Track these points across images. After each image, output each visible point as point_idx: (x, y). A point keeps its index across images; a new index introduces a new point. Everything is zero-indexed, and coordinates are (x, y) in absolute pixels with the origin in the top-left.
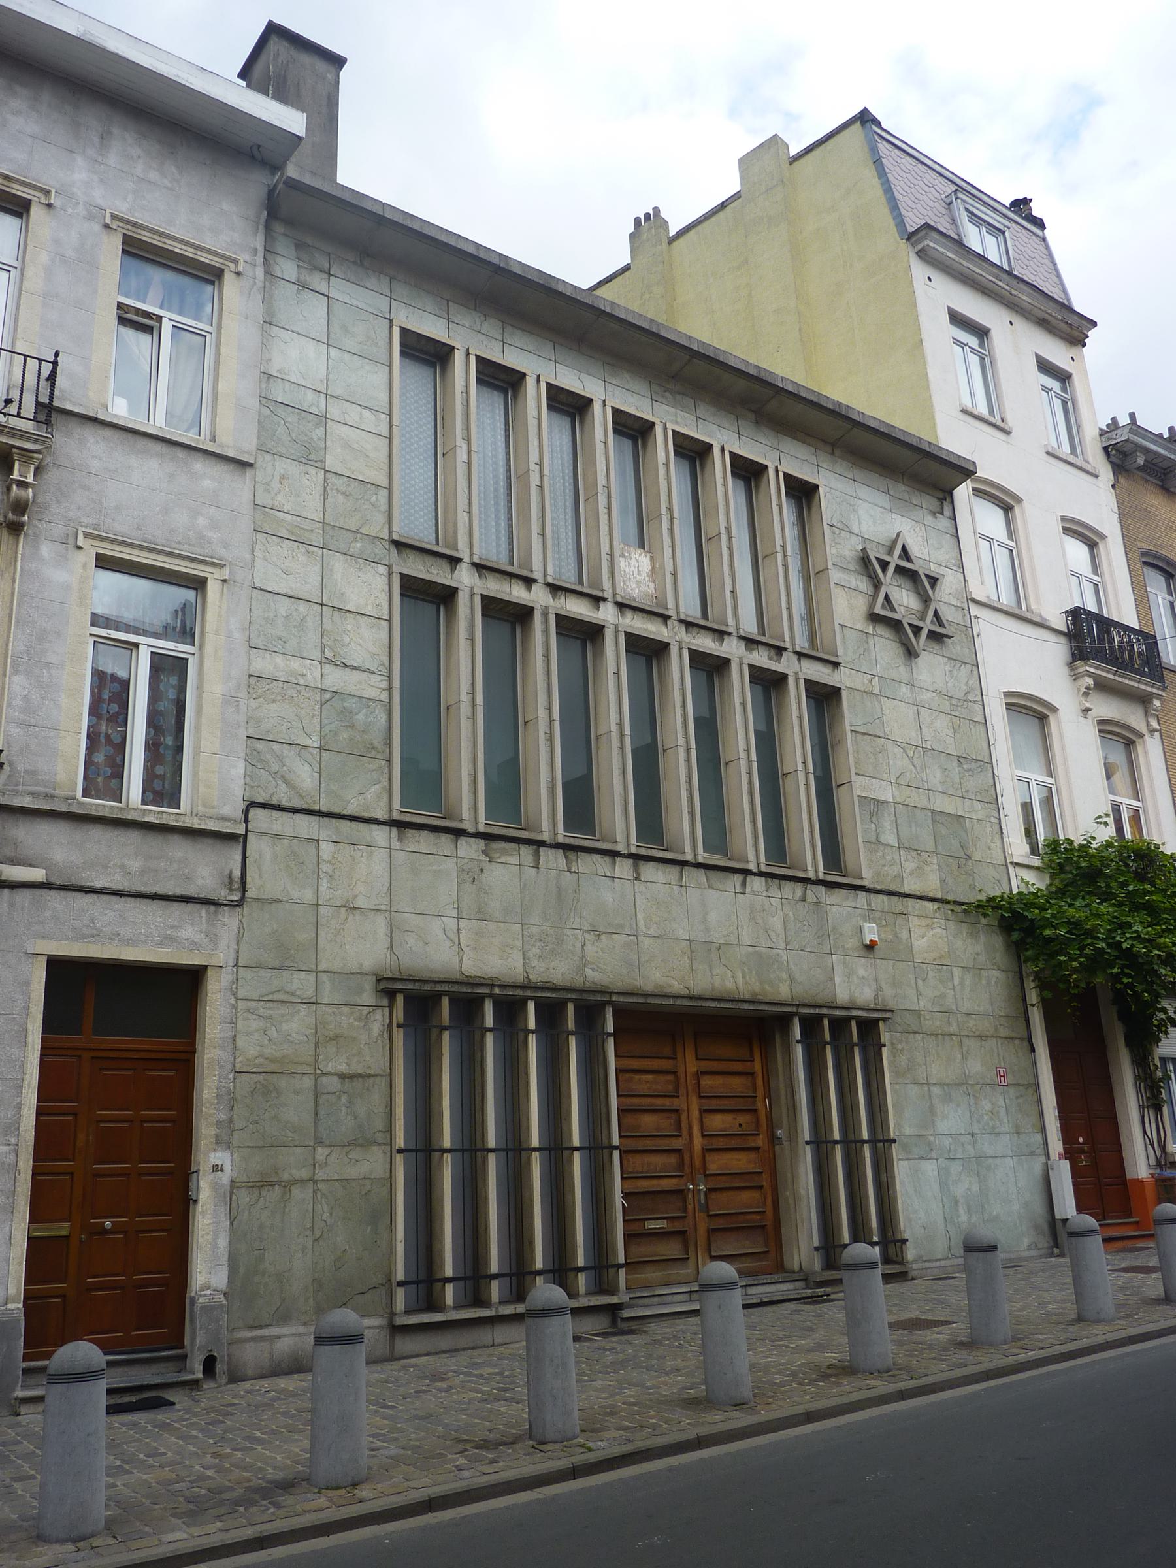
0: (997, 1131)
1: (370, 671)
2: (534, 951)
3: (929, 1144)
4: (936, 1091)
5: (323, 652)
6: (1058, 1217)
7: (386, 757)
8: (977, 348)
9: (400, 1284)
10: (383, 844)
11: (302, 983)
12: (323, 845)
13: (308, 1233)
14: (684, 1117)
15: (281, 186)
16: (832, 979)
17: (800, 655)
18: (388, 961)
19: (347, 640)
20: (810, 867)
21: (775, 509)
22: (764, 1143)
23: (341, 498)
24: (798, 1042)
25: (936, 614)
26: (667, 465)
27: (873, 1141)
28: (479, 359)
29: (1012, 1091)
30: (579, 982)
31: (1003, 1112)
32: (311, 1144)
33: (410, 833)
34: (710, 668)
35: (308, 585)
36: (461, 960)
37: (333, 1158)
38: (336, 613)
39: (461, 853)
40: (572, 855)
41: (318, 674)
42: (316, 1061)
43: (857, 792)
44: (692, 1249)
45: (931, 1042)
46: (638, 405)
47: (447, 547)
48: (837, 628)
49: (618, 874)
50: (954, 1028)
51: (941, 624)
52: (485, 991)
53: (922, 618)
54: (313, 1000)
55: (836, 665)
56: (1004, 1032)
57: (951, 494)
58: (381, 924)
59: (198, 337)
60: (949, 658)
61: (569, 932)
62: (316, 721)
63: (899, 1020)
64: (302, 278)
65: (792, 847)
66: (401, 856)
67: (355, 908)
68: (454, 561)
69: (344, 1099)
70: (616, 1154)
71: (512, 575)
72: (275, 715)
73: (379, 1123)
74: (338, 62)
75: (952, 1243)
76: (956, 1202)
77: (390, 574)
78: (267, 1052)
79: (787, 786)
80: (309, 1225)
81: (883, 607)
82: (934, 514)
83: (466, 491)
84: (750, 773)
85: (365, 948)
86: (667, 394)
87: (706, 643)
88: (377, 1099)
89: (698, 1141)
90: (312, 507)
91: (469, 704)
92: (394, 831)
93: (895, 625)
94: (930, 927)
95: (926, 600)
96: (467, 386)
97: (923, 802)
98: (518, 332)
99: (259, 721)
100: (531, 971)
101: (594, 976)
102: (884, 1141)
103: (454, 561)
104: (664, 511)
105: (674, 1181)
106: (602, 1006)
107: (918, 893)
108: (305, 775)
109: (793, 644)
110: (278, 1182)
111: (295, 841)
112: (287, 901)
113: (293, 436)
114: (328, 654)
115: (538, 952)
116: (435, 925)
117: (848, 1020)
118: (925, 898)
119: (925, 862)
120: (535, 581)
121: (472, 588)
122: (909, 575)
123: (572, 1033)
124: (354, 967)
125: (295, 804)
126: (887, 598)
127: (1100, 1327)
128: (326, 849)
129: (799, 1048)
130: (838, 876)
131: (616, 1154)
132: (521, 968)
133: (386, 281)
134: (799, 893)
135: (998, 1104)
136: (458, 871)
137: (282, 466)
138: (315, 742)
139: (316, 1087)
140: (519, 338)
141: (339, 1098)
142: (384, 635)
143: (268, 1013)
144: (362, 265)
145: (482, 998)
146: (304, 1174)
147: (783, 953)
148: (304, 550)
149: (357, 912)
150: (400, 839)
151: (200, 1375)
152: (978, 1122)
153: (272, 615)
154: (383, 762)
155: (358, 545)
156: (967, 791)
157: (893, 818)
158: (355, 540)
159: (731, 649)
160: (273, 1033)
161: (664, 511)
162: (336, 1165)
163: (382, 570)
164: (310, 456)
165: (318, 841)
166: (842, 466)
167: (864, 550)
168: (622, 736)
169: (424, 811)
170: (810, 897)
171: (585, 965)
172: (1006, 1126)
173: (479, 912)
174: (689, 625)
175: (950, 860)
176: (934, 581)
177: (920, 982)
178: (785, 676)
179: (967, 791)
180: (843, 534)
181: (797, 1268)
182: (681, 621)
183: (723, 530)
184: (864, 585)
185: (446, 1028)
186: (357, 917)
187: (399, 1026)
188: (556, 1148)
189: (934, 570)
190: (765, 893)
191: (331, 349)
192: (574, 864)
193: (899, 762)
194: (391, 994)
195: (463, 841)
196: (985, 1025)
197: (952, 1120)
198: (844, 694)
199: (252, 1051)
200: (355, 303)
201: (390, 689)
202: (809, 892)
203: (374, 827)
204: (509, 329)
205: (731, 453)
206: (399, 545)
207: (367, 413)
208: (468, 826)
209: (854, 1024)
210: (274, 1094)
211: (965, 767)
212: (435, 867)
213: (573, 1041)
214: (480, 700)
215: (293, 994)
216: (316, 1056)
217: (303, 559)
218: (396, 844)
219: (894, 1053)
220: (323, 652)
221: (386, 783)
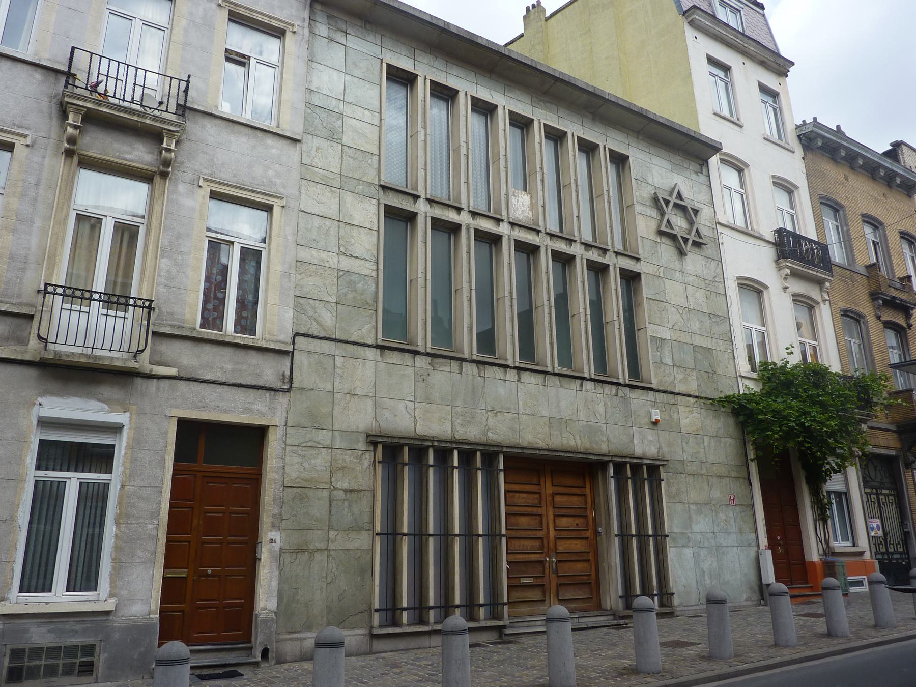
1: (366, 260)
3: (688, 538)
4: (693, 507)
5: (339, 248)
9: (376, 610)
11: (323, 437)
12: (337, 358)
16: (633, 442)
17: (617, 254)
19: (353, 241)
20: (620, 376)
23: (351, 161)
25: (697, 231)
26: (540, 143)
27: (655, 536)
29: (738, 509)
31: (732, 521)
33: (387, 352)
34: (564, 261)
35: (332, 211)
37: (339, 537)
38: (347, 226)
40: (481, 367)
41: (336, 260)
43: (650, 333)
45: (691, 479)
46: (524, 108)
47: (412, 189)
50: (704, 471)
51: (700, 237)
53: (689, 233)
55: (638, 260)
56: (733, 474)
58: (370, 404)
61: (478, 411)
62: (335, 287)
63: (671, 466)
65: (610, 365)
66: (382, 366)
68: (416, 197)
69: (346, 503)
70: (504, 539)
71: (449, 206)
72: (311, 284)
73: (366, 518)
77: (379, 204)
78: (303, 475)
79: (608, 329)
81: (666, 226)
82: (697, 173)
84: (586, 322)
85: (361, 418)
87: (562, 247)
89: (552, 533)
91: (423, 279)
92: (378, 351)
93: (673, 237)
95: (691, 223)
97: (688, 341)
98: (455, 66)
99: (302, 286)
100: (456, 433)
101: (493, 437)
103: (416, 197)
104: (538, 169)
105: (538, 556)
110: (307, 550)
114: (342, 249)
116: (401, 406)
117: (641, 465)
119: (689, 375)
120: (462, 209)
122: (681, 208)
124: (354, 428)
125: (322, 334)
126: (668, 221)
128: (339, 361)
130: (636, 381)
131: (504, 539)
134: (614, 391)
137: (317, 142)
140: (456, 70)
146: (323, 546)
158: (359, 185)
159: (576, 250)
160: (306, 465)
161: (538, 169)
162: (340, 541)
163: (374, 202)
164: (333, 136)
167: (655, 194)
169: (395, 341)
170: (621, 393)
172: (733, 528)
174: (551, 235)
176: (696, 212)
180: (643, 184)
181: (609, 608)
182: (547, 233)
184: (655, 214)
185: (406, 464)
187: (379, 462)
188: (469, 535)
189: (696, 205)
193: (674, 317)
194: (375, 444)
195: (418, 357)
196: (723, 470)
197: (701, 525)
198: (643, 276)
200: (361, 49)
201: (377, 270)
202: (620, 391)
203: (367, 348)
204: (450, 65)
206: (384, 188)
207: (367, 112)
208: (421, 348)
209: (645, 468)
213: (479, 473)
215: (318, 443)
216: (331, 478)
217: (329, 195)
218: (379, 359)
219: (669, 485)
220: (339, 248)
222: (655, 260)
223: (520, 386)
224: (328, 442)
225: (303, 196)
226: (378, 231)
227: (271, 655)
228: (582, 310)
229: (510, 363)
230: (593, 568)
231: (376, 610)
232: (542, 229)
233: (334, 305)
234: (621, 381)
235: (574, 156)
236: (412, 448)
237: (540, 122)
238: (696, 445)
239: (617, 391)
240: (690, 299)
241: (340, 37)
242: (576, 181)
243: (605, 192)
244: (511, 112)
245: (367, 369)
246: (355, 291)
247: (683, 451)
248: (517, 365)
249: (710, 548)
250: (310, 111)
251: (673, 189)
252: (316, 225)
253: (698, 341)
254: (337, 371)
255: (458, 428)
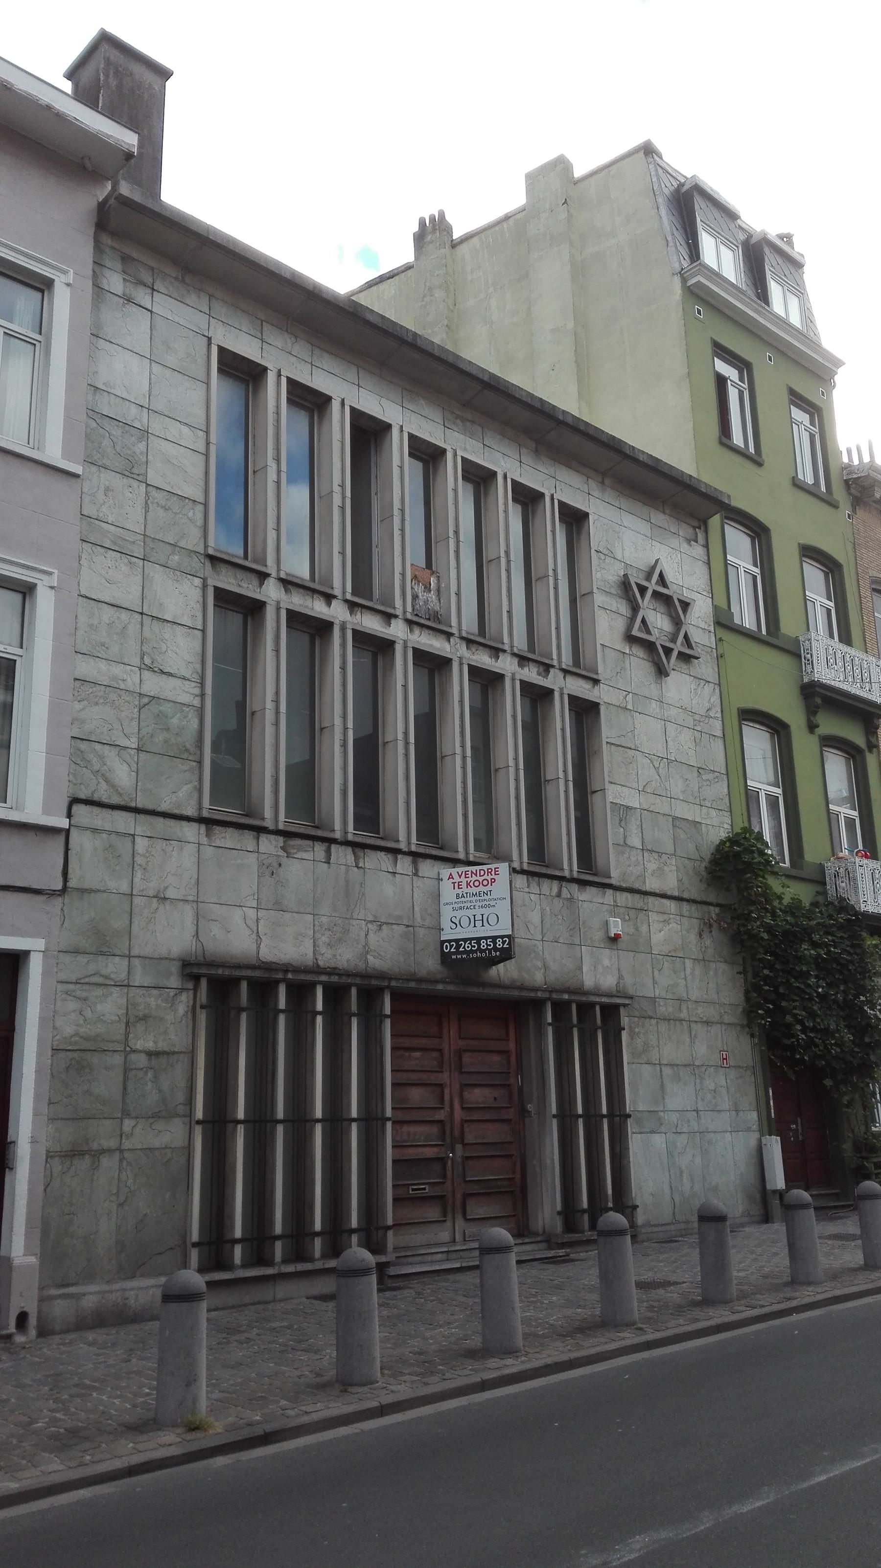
0: (719, 1108)
1: (184, 678)
2: (324, 939)
3: (659, 1119)
4: (667, 1071)
5: (142, 658)
6: (769, 1187)
7: (197, 758)
8: (737, 381)
9: (194, 1245)
10: (192, 839)
11: (115, 967)
12: (138, 840)
13: (112, 1198)
14: (447, 1091)
15: (112, 201)
16: (580, 968)
17: (566, 672)
18: (194, 947)
19: (164, 648)
20: (566, 866)
21: (549, 534)
22: (517, 1112)
23: (161, 513)
24: (549, 1024)
25: (686, 637)
26: (455, 490)
27: (611, 1115)
28: (290, 381)
29: (733, 1074)
30: (362, 966)
31: (724, 1091)
32: (119, 1115)
33: (217, 829)
34: (486, 682)
35: (129, 595)
36: (259, 947)
37: (138, 1130)
38: (155, 622)
39: (262, 849)
40: (360, 853)
41: (136, 679)
42: (127, 1039)
43: (610, 798)
44: (450, 1215)
45: (663, 1027)
46: (432, 431)
47: (255, 561)
48: (599, 647)
49: (399, 869)
50: (684, 1015)
51: (690, 646)
52: (280, 976)
53: (674, 640)
54: (125, 983)
55: (596, 682)
56: (727, 1019)
57: (705, 524)
58: (188, 912)
59: (29, 345)
60: (695, 677)
61: (354, 922)
62: (135, 724)
63: (636, 1006)
64: (128, 292)
65: (551, 847)
66: (208, 851)
67: (165, 899)
68: (263, 576)
69: (150, 1075)
70: (389, 1125)
71: (314, 591)
72: (96, 717)
73: (180, 1097)
74: (165, 74)
75: (677, 1210)
76: (681, 1172)
77: (205, 586)
78: (82, 1030)
79: (549, 791)
80: (115, 1191)
81: (640, 630)
82: (689, 541)
83: (275, 509)
84: (517, 780)
85: (172, 934)
86: (458, 421)
87: (484, 660)
88: (179, 1071)
89: (458, 1114)
90: (134, 521)
91: (273, 711)
92: (203, 828)
93: (649, 646)
94: (667, 922)
95: (677, 623)
96: (278, 407)
97: (666, 809)
98: (325, 355)
99: (83, 722)
100: (320, 958)
101: (375, 963)
102: (620, 1116)
103: (263, 576)
104: (451, 534)
105: (435, 1150)
106: (381, 990)
107: (657, 891)
108: (122, 774)
109: (560, 662)
110: (89, 1152)
111: (113, 836)
112: (104, 891)
113: (118, 448)
114: (147, 661)
115: (327, 940)
116: (237, 914)
117: (593, 1005)
118: (664, 896)
119: (665, 864)
120: (335, 597)
121: (278, 603)
122: (664, 600)
123: (354, 1015)
124: (163, 952)
125: (115, 800)
126: (644, 621)
127: (810, 1289)
128: (141, 844)
129: (550, 1030)
130: (590, 873)
131: (389, 1125)
132: (311, 954)
133: (205, 298)
134: (555, 890)
135: (718, 1081)
136: (259, 866)
137: (107, 478)
138: (133, 743)
139: (125, 1063)
140: (327, 362)
141: (146, 1073)
142: (197, 645)
143: (85, 994)
144: (183, 281)
145: (277, 982)
146: (113, 1143)
147: (539, 944)
148: (126, 561)
149: (168, 901)
150: (208, 835)
151: (14, 1330)
152: (703, 1100)
153: (96, 623)
154: (194, 764)
155: (177, 557)
156: (704, 800)
157: (639, 823)
158: (173, 553)
159: (506, 665)
160: (88, 1014)
161: (451, 534)
162: (143, 1136)
163: (197, 582)
164: (132, 470)
165: (133, 835)
166: (610, 495)
167: (625, 576)
168: (407, 743)
169: (231, 812)
170: (565, 893)
171: (367, 953)
172: (725, 1104)
173: (276, 903)
174: (469, 642)
175: (687, 862)
176: (685, 605)
177: (656, 972)
178: (551, 691)
179: (704, 800)
180: (608, 560)
181: (540, 1231)
182: (462, 638)
183: (502, 554)
184: (623, 608)
185: (243, 1010)
186: (168, 907)
187: (202, 1007)
188: (336, 1120)
189: (687, 595)
190: (527, 890)
191: (154, 364)
192: (361, 860)
193: (646, 772)
194: (196, 978)
195: (264, 838)
196: (711, 1012)
197: (679, 1097)
198: (602, 708)
199: (68, 1030)
200: (177, 319)
201: (202, 695)
202: (564, 890)
203: (185, 823)
204: (317, 352)
205: (512, 480)
206: (214, 560)
207: (185, 430)
208: (269, 824)
209: (598, 1008)
210: (87, 1070)
211: (704, 777)
212: (239, 861)
213: (354, 1022)
214: (283, 708)
215: (107, 977)
216: (127, 1034)
217: (124, 568)
218: (204, 840)
219: (632, 1035)
220: (142, 658)
221: (196, 783)
222: (621, 680)
223: (418, 882)
224: (123, 976)
225: (85, 571)
226: (203, 631)
227: (32, 1321)
228: (511, 763)
229: (403, 846)
230: (518, 1168)
231: (194, 1245)
232: (454, 630)
233: (133, 752)
234: (567, 874)
235: (506, 511)
236: (252, 982)
237: (455, 455)
238: (660, 963)
239: (560, 891)
240: (670, 743)
241: (143, 296)
242: (507, 553)
243: (551, 573)
244: (411, 437)
245: (180, 858)
246: (168, 729)
247: (655, 982)
248: (413, 848)
249: (692, 1133)
250: (94, 424)
251: (653, 568)
252: (105, 618)
253: (682, 811)
254: (139, 860)
255: (323, 949)
